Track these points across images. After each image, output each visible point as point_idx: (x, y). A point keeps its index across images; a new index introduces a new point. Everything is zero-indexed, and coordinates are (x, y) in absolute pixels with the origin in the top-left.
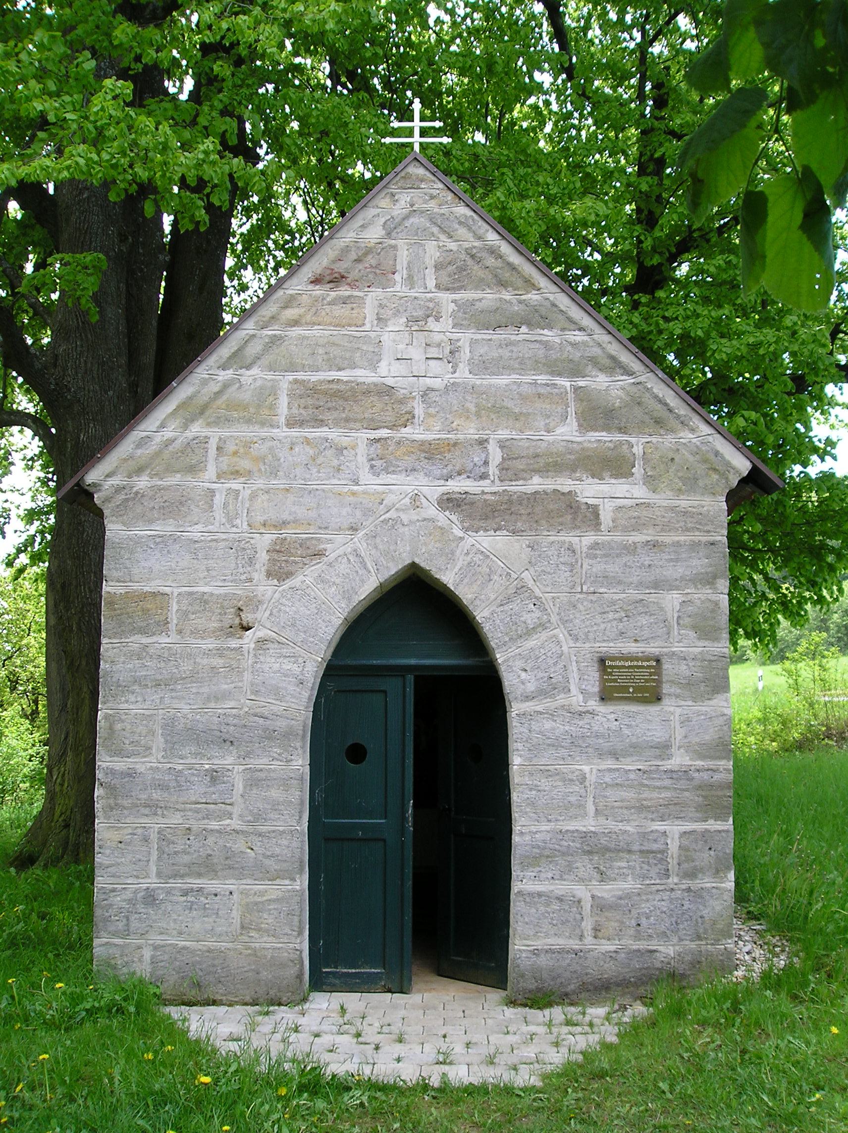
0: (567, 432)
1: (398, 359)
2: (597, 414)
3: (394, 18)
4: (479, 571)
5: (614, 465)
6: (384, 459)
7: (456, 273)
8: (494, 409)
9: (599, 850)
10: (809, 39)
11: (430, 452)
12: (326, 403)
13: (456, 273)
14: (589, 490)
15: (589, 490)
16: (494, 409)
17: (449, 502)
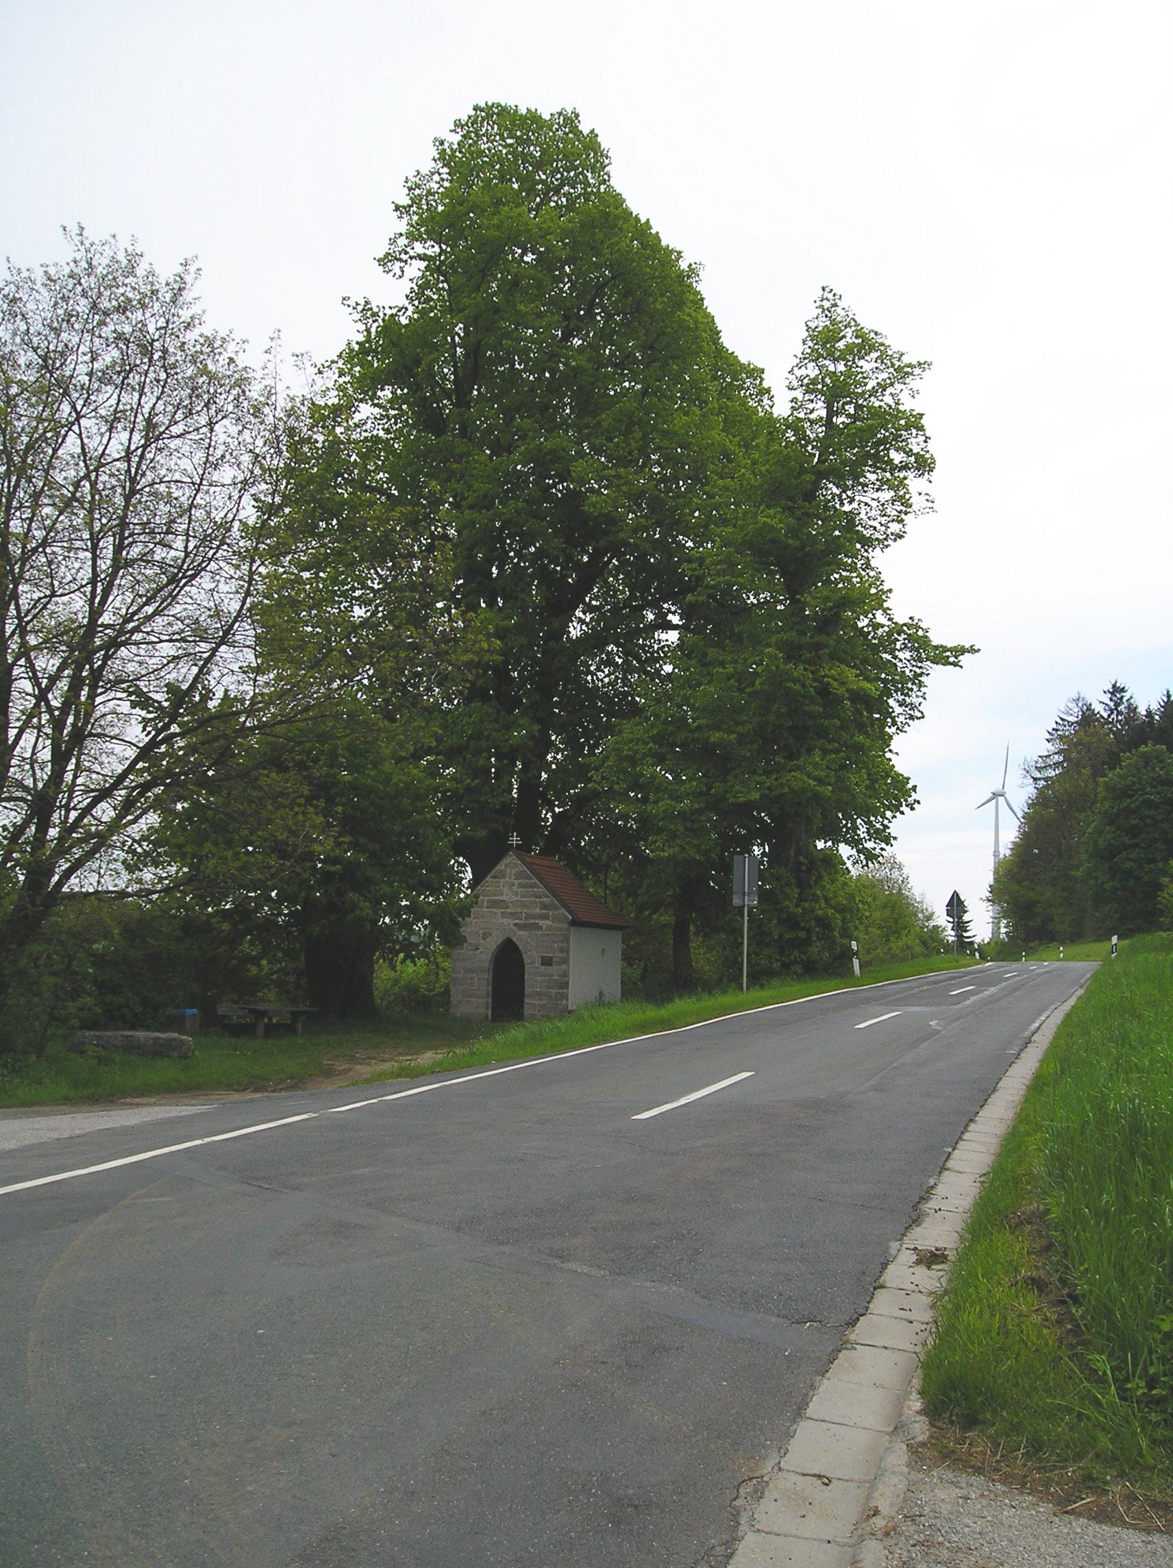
0: (538, 910)
1: (507, 895)
2: (544, 906)
3: (594, 603)
4: (522, 938)
5: (546, 917)
6: (504, 915)
7: (518, 876)
8: (524, 905)
9: (540, 995)
10: (750, 851)
11: (512, 914)
12: (494, 904)
13: (518, 876)
14: (541, 923)
15: (541, 923)
16: (524, 905)
17: (515, 925)
